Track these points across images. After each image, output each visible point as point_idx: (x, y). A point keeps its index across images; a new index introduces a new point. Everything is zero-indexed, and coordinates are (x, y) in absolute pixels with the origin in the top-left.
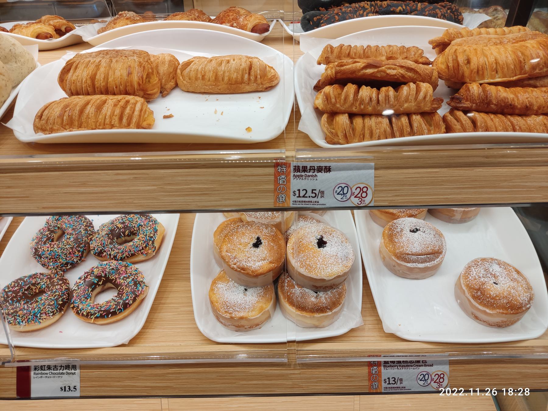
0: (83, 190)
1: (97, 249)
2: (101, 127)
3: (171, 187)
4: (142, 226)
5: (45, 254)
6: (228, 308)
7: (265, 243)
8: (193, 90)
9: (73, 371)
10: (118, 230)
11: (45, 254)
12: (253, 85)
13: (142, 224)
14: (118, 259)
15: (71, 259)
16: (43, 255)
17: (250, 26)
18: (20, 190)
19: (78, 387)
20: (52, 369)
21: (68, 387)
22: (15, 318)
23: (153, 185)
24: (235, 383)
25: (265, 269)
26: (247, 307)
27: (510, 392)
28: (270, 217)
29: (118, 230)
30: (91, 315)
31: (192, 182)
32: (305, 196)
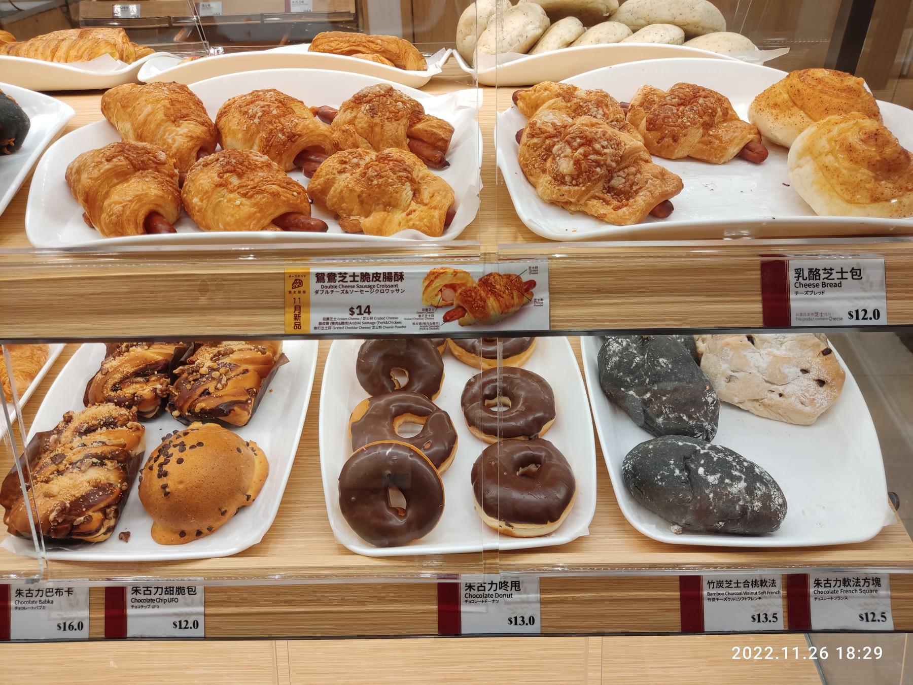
19: (86, 624)
20: (823, 585)
21: (521, 619)
27: (849, 653)
32: (866, 317)
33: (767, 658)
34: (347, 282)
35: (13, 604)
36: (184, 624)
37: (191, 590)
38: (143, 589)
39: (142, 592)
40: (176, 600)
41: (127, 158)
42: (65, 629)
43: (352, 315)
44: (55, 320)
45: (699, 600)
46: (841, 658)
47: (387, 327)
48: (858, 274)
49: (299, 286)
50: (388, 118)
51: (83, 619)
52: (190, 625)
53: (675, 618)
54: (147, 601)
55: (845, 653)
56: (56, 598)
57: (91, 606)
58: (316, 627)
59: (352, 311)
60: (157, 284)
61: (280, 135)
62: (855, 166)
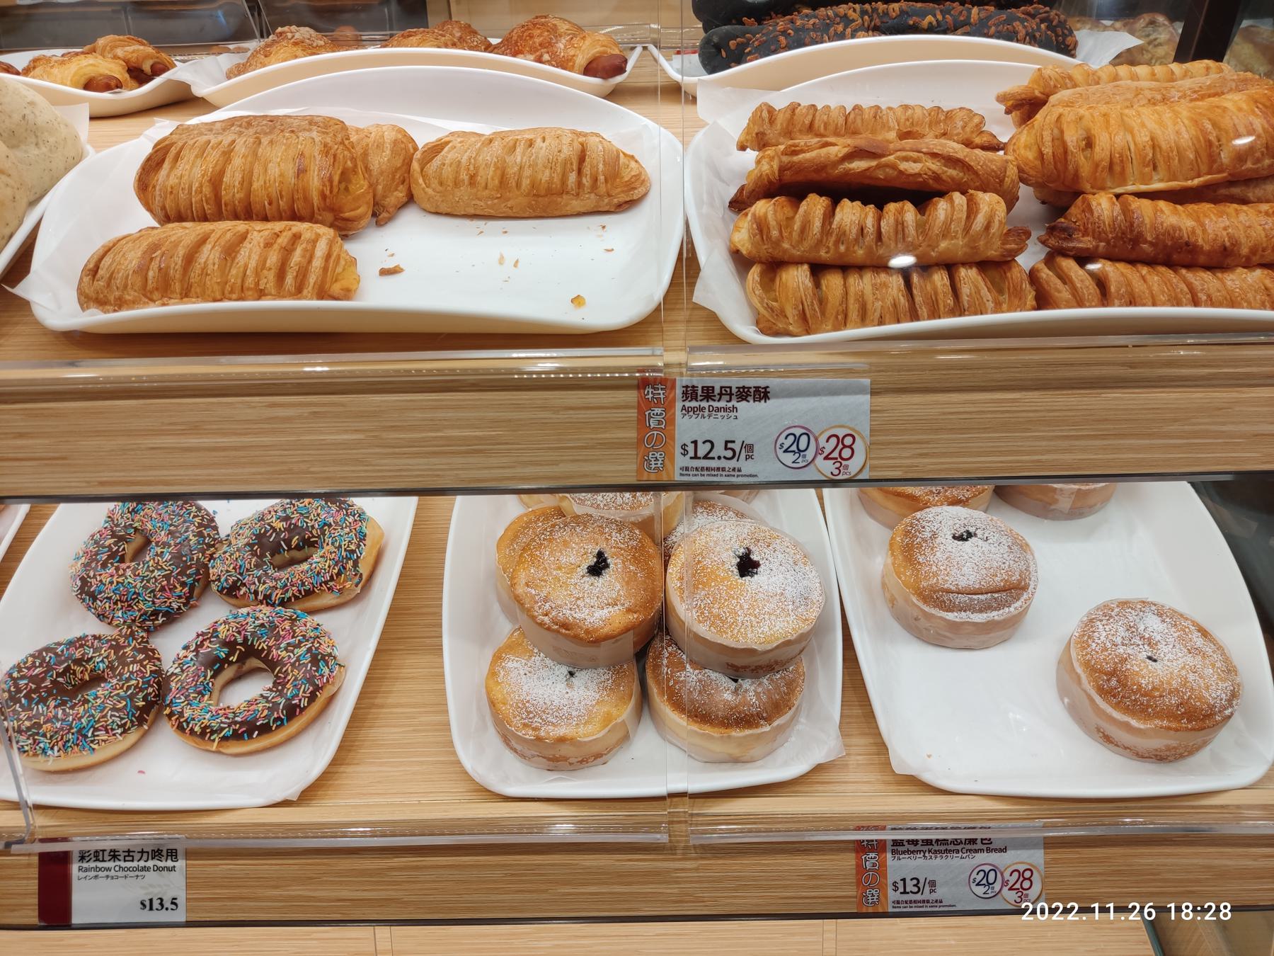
0: (193, 441)
1: (226, 580)
2: (234, 296)
3: (397, 436)
4: (330, 525)
5: (104, 592)
6: (531, 715)
7: (616, 564)
8: (449, 210)
9: (170, 863)
10: (274, 535)
11: (104, 592)
12: (589, 198)
13: (331, 520)
14: (275, 603)
15: (165, 602)
16: (100, 593)
17: (581, 60)
18: (46, 441)
19: (181, 901)
20: (122, 858)
21: (159, 901)
22: (35, 740)
23: (356, 431)
24: (545, 891)
25: (617, 625)
26: (574, 713)
27: (1185, 911)
28: (627, 504)
29: (274, 535)
30: (212, 732)
31: (446, 423)
32: (710, 455)
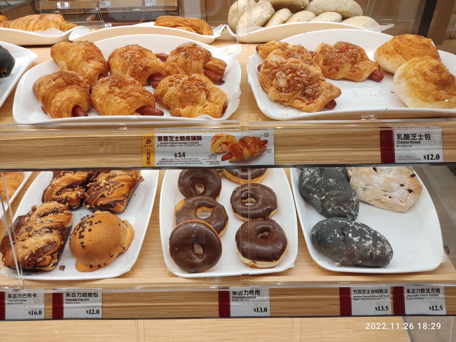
19: (43, 312)
20: (411, 292)
21: (260, 309)
27: (424, 326)
32: (432, 158)
33: (383, 328)
34: (173, 141)
35: (6, 301)
36: (92, 312)
37: (96, 295)
38: (71, 294)
39: (71, 295)
40: (88, 300)
41: (63, 79)
42: (32, 314)
43: (176, 157)
44: (27, 160)
45: (349, 299)
46: (420, 328)
47: (193, 163)
48: (429, 137)
49: (149, 143)
50: (194, 59)
51: (42, 309)
52: (95, 312)
53: (337, 309)
54: (73, 300)
55: (422, 326)
56: (28, 299)
57: (46, 303)
58: (158, 313)
59: (176, 155)
60: (79, 142)
61: (140, 67)
62: (427, 83)
